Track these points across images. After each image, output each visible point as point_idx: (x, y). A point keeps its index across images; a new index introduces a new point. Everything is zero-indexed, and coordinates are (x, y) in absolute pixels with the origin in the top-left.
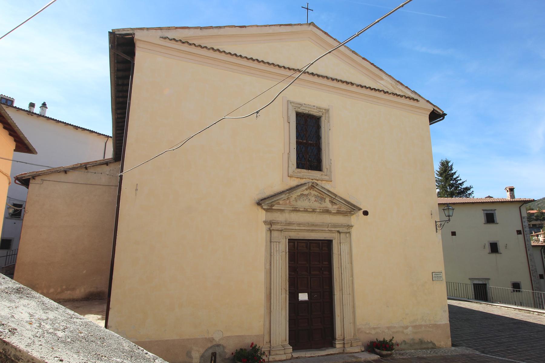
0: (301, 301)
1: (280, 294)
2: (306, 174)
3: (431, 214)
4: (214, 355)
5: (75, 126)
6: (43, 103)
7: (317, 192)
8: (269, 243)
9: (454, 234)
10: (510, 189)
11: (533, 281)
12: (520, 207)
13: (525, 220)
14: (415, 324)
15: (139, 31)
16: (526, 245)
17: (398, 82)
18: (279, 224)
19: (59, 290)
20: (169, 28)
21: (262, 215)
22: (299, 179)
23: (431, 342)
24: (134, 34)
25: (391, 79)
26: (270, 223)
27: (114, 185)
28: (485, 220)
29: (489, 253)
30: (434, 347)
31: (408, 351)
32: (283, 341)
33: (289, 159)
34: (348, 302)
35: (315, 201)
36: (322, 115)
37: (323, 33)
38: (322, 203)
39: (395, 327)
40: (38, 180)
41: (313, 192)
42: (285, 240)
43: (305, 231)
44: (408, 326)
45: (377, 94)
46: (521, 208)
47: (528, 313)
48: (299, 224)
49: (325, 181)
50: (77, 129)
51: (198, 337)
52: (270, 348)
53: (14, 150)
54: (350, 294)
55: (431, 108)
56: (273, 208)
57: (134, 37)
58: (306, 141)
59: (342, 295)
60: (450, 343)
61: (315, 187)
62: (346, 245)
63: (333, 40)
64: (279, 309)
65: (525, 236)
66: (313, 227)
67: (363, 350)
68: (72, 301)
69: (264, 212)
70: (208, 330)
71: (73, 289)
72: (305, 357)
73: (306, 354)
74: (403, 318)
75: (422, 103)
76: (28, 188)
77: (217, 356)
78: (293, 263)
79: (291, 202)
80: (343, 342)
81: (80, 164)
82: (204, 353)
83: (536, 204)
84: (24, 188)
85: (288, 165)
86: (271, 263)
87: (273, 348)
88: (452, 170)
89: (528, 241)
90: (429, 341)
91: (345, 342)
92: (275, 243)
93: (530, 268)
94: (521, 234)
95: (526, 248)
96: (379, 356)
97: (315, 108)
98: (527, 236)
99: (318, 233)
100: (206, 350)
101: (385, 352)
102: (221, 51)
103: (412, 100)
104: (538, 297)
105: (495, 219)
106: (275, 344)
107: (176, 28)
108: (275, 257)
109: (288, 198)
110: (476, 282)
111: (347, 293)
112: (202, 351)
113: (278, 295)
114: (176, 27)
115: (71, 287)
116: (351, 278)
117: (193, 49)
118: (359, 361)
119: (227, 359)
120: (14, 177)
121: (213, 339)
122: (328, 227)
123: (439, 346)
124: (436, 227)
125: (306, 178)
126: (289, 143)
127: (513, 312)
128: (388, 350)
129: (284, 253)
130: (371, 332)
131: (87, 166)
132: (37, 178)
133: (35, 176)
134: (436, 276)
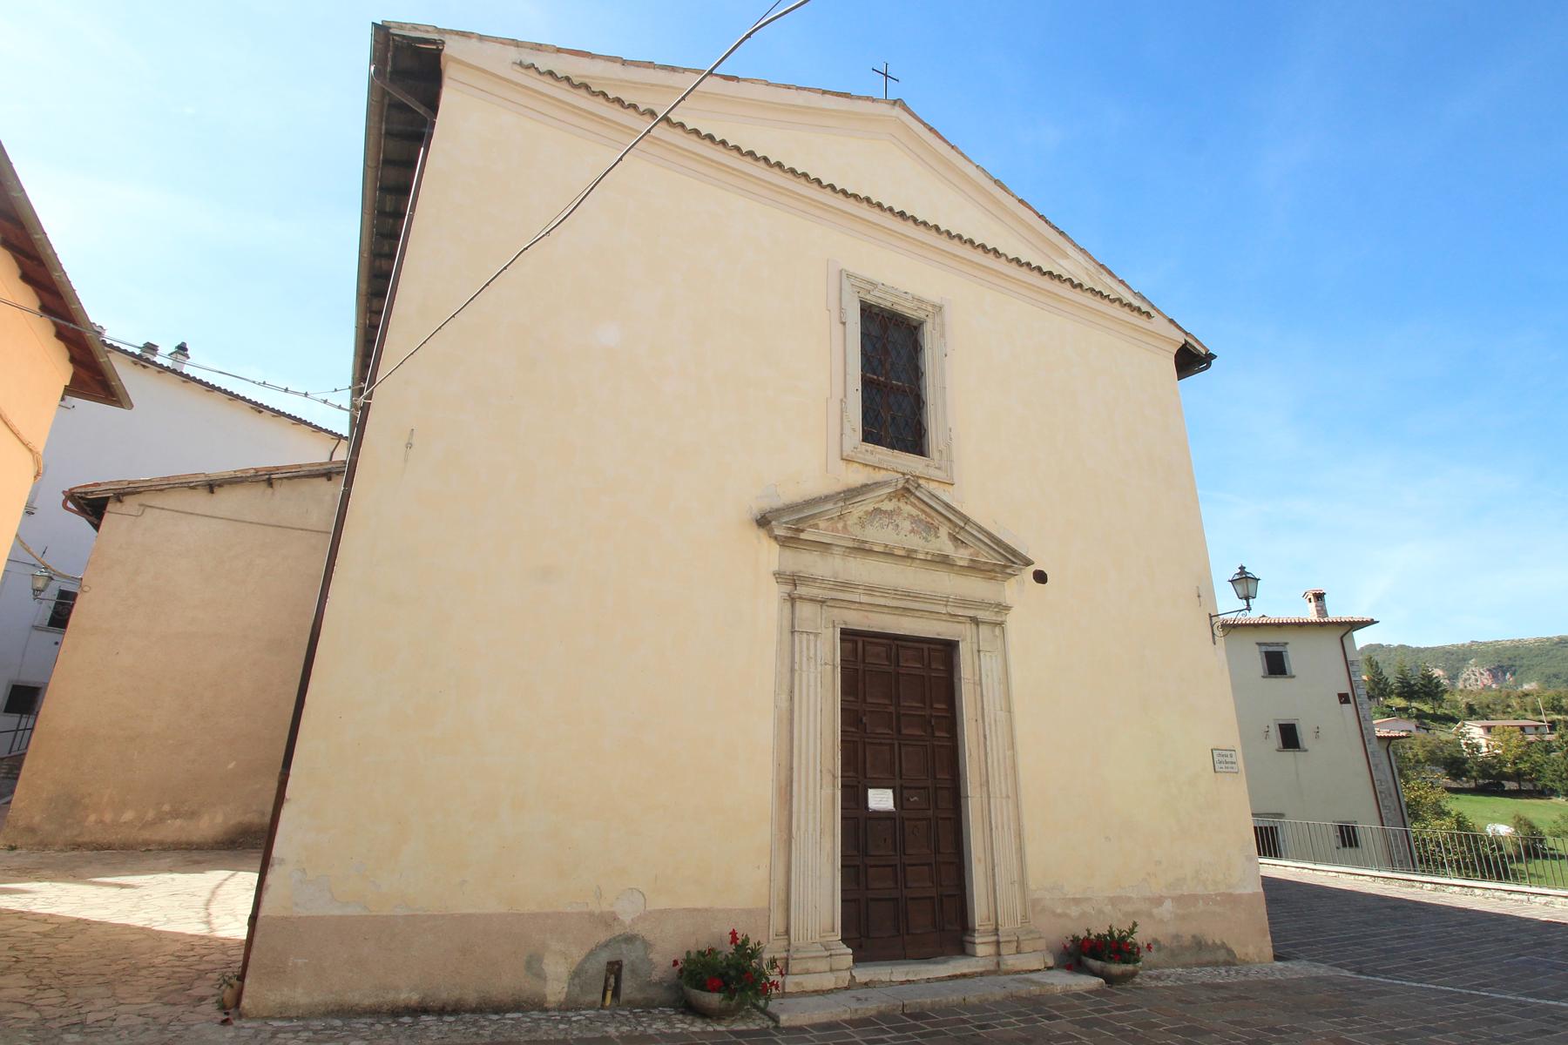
0: (876, 812)
1: (818, 787)
4: (615, 968)
5: (255, 403)
6: (180, 343)
7: (919, 508)
8: (787, 635)
10: (1315, 595)
11: (1384, 819)
12: (1342, 638)
14: (1179, 892)
15: (457, 37)
17: (1102, 266)
18: (817, 585)
19: (151, 815)
20: (538, 47)
21: (770, 555)
22: (871, 469)
23: (1223, 946)
24: (443, 43)
25: (1087, 259)
26: (792, 580)
28: (1264, 668)
30: (1231, 961)
31: (1167, 971)
32: (824, 931)
33: (845, 414)
34: (1005, 818)
35: (912, 531)
39: (1129, 899)
40: (131, 504)
41: (907, 509)
42: (831, 629)
43: (886, 610)
44: (1161, 896)
45: (1054, 286)
46: (1344, 638)
47: (1409, 886)
48: (870, 590)
49: (937, 483)
50: (260, 412)
51: (569, 910)
52: (789, 950)
53: (66, 386)
54: (1008, 797)
55: (1181, 339)
56: (803, 536)
57: (442, 50)
58: (886, 379)
59: (989, 797)
60: (1269, 951)
61: (913, 494)
62: (994, 658)
64: (815, 830)
65: (1359, 707)
66: (908, 601)
68: (186, 849)
69: (775, 547)
70: (599, 888)
71: (193, 815)
72: (891, 981)
73: (892, 972)
74: (1149, 874)
75: (1157, 323)
76: (97, 527)
77: (625, 973)
78: (851, 698)
79: (849, 528)
80: (994, 938)
81: (255, 469)
84: (82, 523)
85: (842, 429)
90: (1218, 942)
91: (1001, 940)
94: (1349, 702)
96: (1101, 980)
97: (909, 297)
98: (1362, 708)
99: (919, 620)
100: (592, 953)
101: (1116, 968)
102: (674, 121)
103: (1135, 313)
104: (1399, 861)
105: (1286, 665)
106: (801, 939)
107: (559, 50)
108: (804, 675)
109: (841, 517)
111: (1001, 794)
112: (578, 955)
113: (811, 789)
114: (558, 46)
115: (186, 808)
116: (1009, 753)
117: (598, 106)
118: (1049, 993)
119: (655, 984)
120: (64, 492)
121: (616, 919)
122: (946, 605)
123: (1243, 958)
124: (1213, 630)
125: (889, 468)
126: (842, 375)
127: (1370, 884)
128: (1127, 962)
129: (829, 668)
130: (1068, 911)
131: (273, 476)
132: (128, 500)
133: (122, 491)
134: (1221, 759)
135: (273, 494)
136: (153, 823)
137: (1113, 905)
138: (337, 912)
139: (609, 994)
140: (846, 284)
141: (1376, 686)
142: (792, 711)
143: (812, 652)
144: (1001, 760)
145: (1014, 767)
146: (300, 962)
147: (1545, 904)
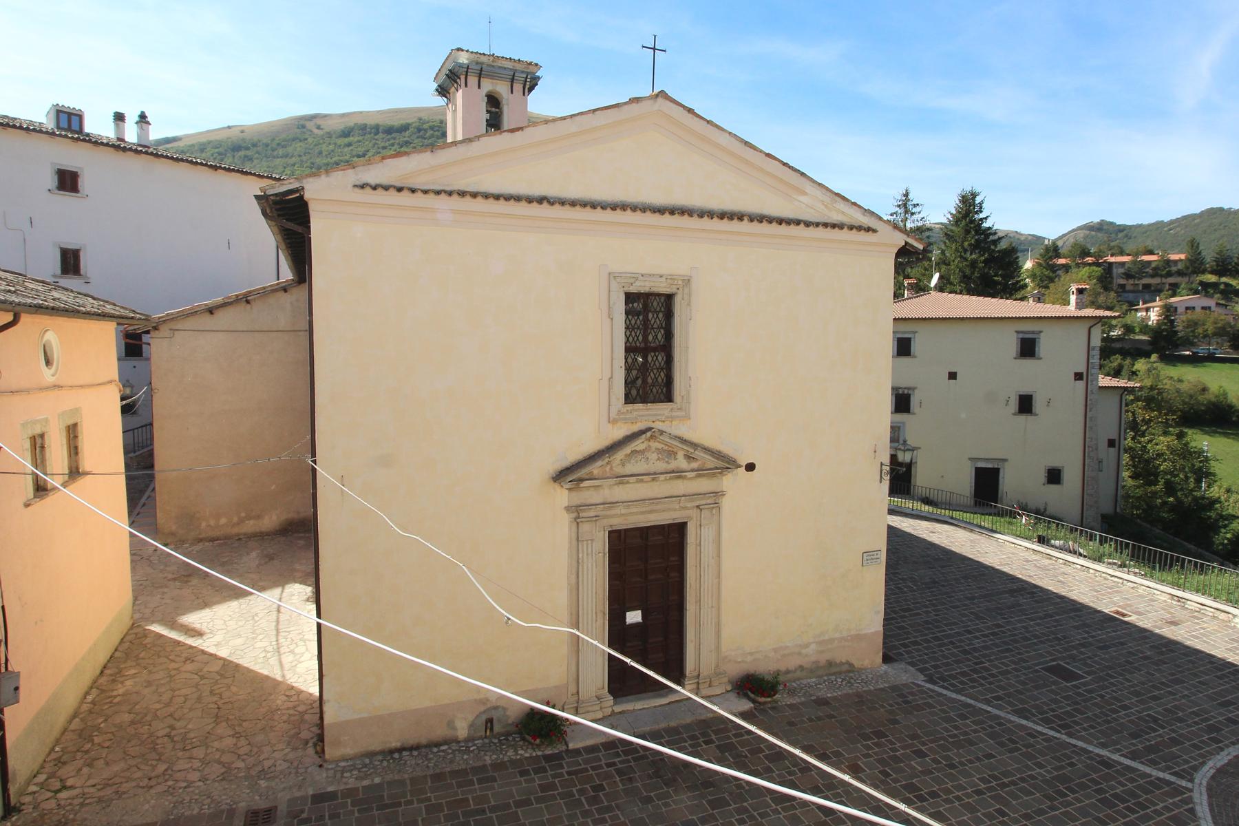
2: (641, 413)
3: (875, 452)
6: (139, 113)
8: (574, 542)
9: (952, 376)
13: (1096, 354)
16: (1088, 399)
19: (235, 519)
21: (562, 496)
23: (848, 663)
24: (303, 188)
26: (576, 511)
27: (302, 329)
29: (1014, 414)
35: (658, 459)
36: (677, 291)
37: (685, 112)
38: (670, 461)
39: (787, 647)
40: (164, 331)
42: (603, 532)
46: (1092, 329)
47: (1048, 558)
54: (712, 607)
59: (700, 609)
63: (706, 123)
67: (729, 689)
77: (494, 721)
79: (614, 469)
80: (696, 681)
82: (474, 720)
83: (1165, 229)
86: (578, 573)
87: (583, 702)
88: (981, 212)
89: (1093, 393)
91: (700, 682)
92: (585, 542)
93: (1087, 443)
95: (1086, 406)
105: (1037, 349)
108: (585, 565)
110: (981, 465)
112: (471, 718)
121: (488, 700)
134: (869, 558)
135: (251, 308)
136: (238, 524)
137: (775, 652)
138: (359, 716)
139: (488, 731)
140: (614, 285)
141: (1191, 264)
142: (578, 583)
143: (590, 550)
144: (710, 588)
145: (719, 589)
146: (346, 738)
147: (1132, 588)
